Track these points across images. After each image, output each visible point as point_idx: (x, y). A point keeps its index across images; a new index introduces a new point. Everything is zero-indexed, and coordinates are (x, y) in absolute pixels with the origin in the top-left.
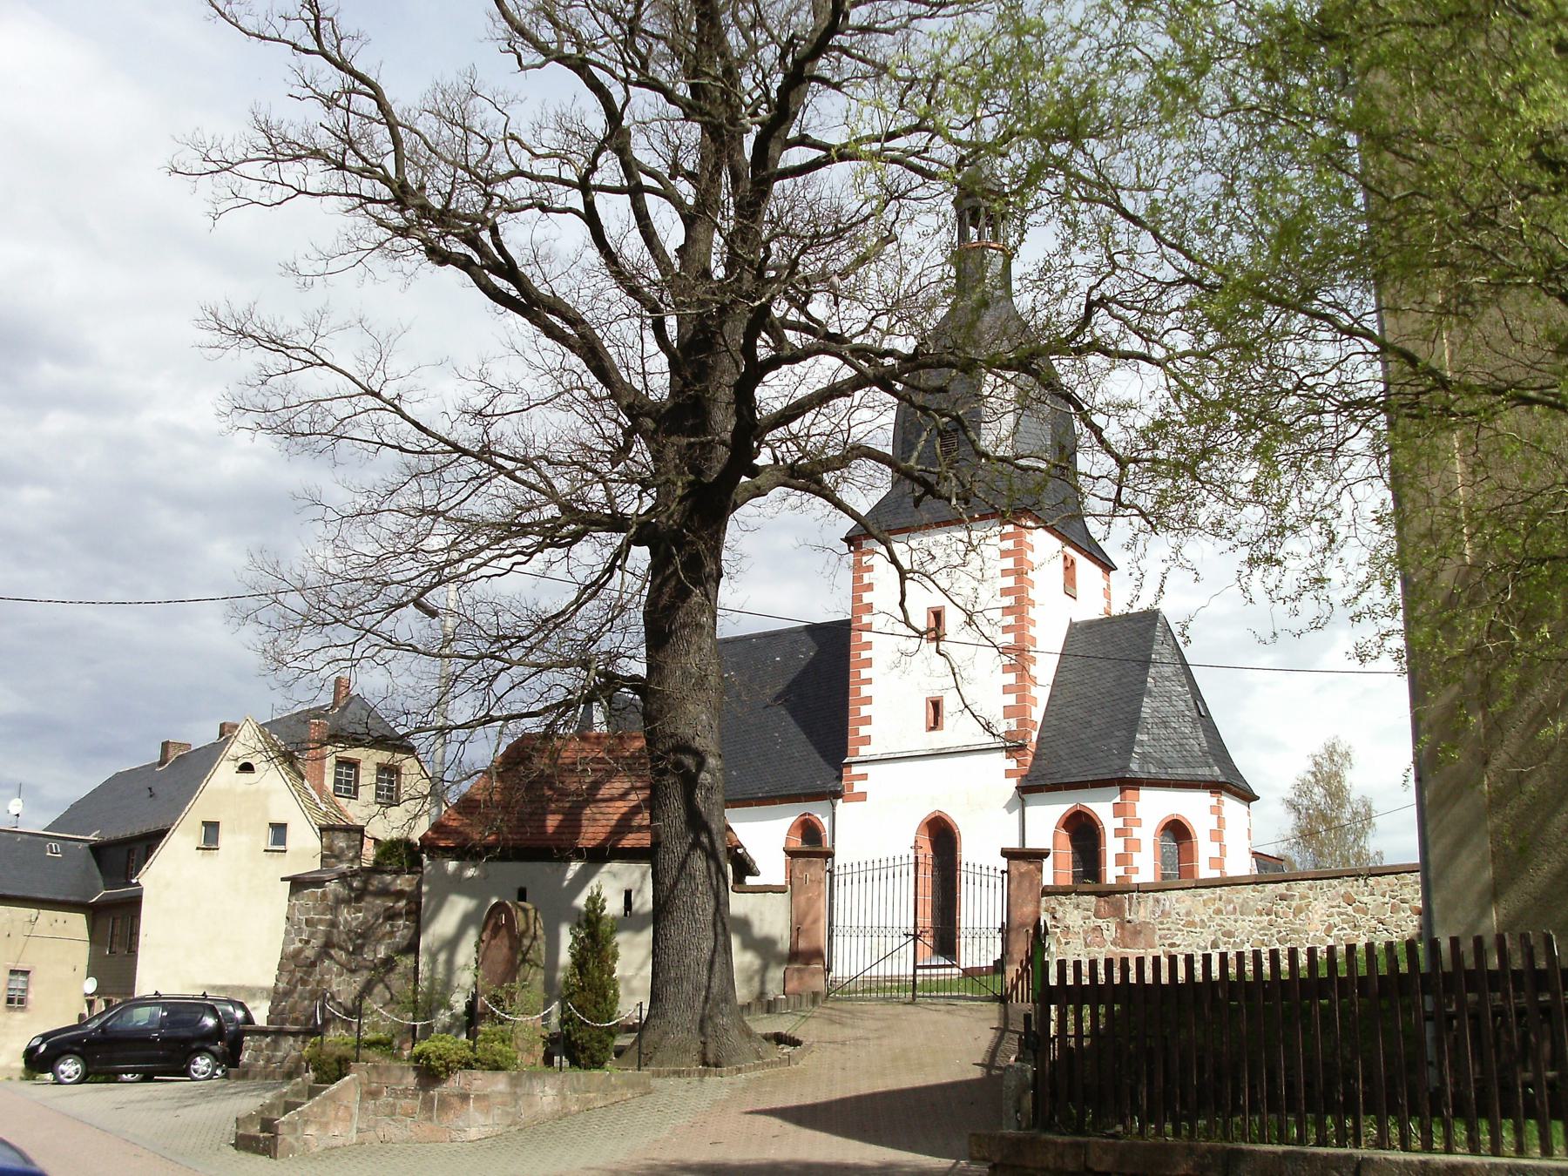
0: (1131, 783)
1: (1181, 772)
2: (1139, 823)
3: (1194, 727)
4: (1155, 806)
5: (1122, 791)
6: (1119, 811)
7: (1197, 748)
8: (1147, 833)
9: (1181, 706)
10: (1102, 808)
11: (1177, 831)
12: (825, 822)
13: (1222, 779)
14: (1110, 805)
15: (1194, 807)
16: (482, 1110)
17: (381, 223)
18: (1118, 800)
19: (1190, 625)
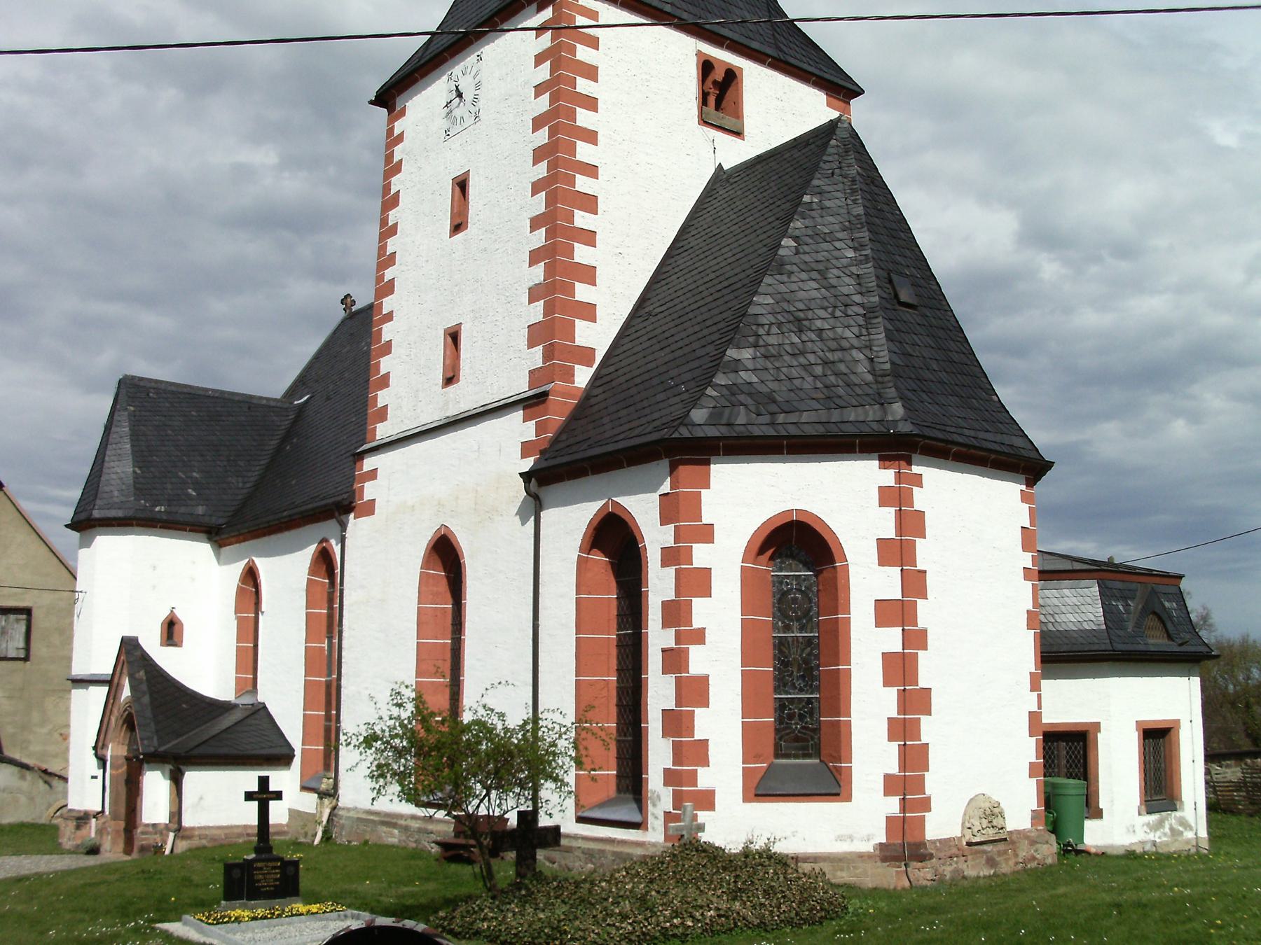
0: (693, 452)
1: (808, 420)
2: (706, 533)
3: (868, 325)
4: (745, 497)
5: (673, 469)
6: (670, 511)
7: (862, 368)
8: (725, 558)
9: (848, 286)
10: (643, 509)
11: (797, 547)
12: (337, 549)
13: (905, 428)
14: (654, 498)
15: (843, 495)
16: (463, 942)
17: (540, 30)
18: (666, 487)
19: (445, 124)
